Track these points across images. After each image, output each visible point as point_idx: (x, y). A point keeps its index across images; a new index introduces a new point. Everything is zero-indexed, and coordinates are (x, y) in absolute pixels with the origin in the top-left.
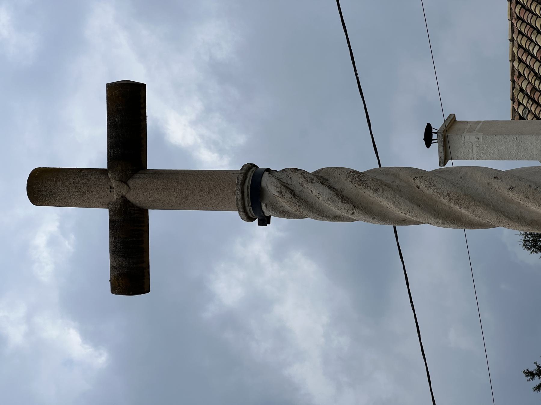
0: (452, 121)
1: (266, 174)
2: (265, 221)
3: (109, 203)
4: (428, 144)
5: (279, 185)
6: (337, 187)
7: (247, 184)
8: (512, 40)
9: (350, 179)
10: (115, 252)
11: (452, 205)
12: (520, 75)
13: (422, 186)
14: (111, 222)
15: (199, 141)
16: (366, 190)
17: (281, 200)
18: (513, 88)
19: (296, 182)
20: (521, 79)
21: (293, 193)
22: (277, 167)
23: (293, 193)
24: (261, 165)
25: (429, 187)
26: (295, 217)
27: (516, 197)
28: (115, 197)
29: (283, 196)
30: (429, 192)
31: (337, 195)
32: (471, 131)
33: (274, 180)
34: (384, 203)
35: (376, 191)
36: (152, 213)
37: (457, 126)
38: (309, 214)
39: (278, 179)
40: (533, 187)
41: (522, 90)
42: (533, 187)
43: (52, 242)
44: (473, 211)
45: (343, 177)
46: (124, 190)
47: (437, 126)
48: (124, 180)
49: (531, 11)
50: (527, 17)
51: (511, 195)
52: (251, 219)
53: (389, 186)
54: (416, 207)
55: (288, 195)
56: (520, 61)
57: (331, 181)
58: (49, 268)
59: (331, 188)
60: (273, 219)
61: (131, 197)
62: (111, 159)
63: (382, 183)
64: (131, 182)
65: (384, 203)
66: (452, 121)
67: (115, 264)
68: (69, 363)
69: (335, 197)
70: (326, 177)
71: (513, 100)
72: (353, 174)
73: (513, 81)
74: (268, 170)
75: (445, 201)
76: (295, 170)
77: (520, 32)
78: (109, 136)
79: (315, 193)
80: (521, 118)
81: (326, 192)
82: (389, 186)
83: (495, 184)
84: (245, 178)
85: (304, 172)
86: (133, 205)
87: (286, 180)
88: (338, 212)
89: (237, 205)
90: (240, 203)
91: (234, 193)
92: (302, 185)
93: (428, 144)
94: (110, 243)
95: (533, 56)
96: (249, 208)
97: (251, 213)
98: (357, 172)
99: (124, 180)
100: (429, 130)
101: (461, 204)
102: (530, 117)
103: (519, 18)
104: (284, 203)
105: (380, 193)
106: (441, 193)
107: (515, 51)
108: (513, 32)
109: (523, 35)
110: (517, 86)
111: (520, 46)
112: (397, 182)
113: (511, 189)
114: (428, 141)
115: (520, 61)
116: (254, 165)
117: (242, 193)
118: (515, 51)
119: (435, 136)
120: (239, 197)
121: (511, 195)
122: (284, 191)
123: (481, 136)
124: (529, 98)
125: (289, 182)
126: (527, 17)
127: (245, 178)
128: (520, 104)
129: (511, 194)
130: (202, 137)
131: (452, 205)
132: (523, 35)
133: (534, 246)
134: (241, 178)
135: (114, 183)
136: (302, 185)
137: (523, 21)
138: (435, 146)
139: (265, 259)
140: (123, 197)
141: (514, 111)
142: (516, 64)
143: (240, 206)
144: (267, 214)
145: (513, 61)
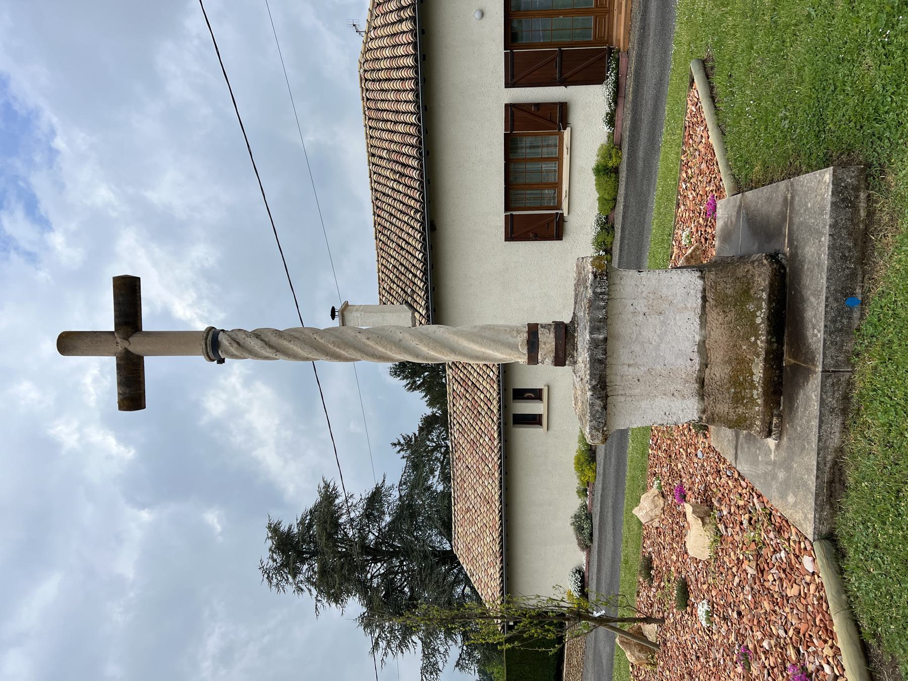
0: (346, 305)
1: (221, 333)
2: (221, 361)
3: (116, 353)
4: (333, 319)
5: (230, 339)
6: (266, 339)
7: (209, 339)
8: (378, 261)
9: (274, 335)
10: (120, 384)
11: (335, 348)
12: (383, 280)
13: (318, 338)
14: (118, 365)
15: (195, 316)
16: (284, 341)
17: (231, 348)
18: (380, 287)
19: (241, 337)
20: (384, 282)
21: (238, 343)
22: (228, 328)
23: (238, 343)
24: (218, 328)
25: (322, 338)
26: (241, 358)
27: (370, 343)
28: (120, 349)
29: (232, 346)
30: (322, 341)
31: (266, 344)
32: (357, 310)
33: (226, 336)
34: (295, 348)
35: (290, 341)
36: (145, 358)
37: (349, 308)
38: (249, 356)
39: (229, 336)
40: (380, 337)
41: (384, 288)
42: (380, 337)
43: (96, 380)
44: (347, 352)
45: (269, 334)
46: (126, 344)
47: (337, 308)
48: (126, 338)
49: (387, 245)
50: (386, 248)
51: (368, 342)
52: (213, 360)
53: (298, 338)
54: (314, 350)
55: (235, 345)
56: (383, 272)
57: (263, 336)
58: (93, 398)
59: (262, 340)
60: (226, 360)
61: (132, 349)
62: (116, 325)
63: (293, 336)
64: (131, 339)
65: (295, 348)
66: (346, 305)
67: (121, 392)
68: (109, 457)
69: (264, 346)
70: (259, 334)
71: (380, 294)
72: (277, 333)
73: (380, 284)
74: (223, 331)
75: (331, 346)
76: (240, 330)
77: (382, 257)
78: (115, 310)
79: (253, 343)
80: (384, 304)
81: (259, 343)
82: (298, 338)
83: (359, 336)
84: (207, 335)
85: (245, 331)
86: (132, 354)
87: (234, 336)
88: (267, 354)
89: (203, 352)
90: (204, 351)
91: (201, 345)
92: (244, 339)
93: (333, 319)
94: (118, 378)
95: (389, 270)
96: (211, 354)
97: (212, 357)
98: (278, 331)
99: (126, 338)
100: (333, 309)
101: (340, 348)
102: (389, 303)
103: (381, 249)
104: (233, 350)
105: (292, 342)
106: (329, 342)
107: (380, 267)
108: (378, 256)
109: (384, 258)
110: (381, 286)
111: (382, 264)
112: (303, 336)
113: (368, 339)
114: (333, 316)
115: (383, 272)
116: (214, 328)
117: (206, 344)
118: (380, 267)
119: (337, 314)
120: (204, 347)
121: (368, 342)
122: (232, 343)
123: (362, 313)
124: (388, 293)
125: (236, 337)
126: (386, 248)
127: (207, 335)
128: (383, 296)
129: (368, 341)
130: (196, 314)
131: (335, 348)
132: (384, 258)
133: (395, 374)
134: (205, 335)
135: (119, 340)
136: (244, 339)
137: (384, 251)
138: (337, 319)
139: (238, 386)
140: (125, 349)
141: (381, 300)
142: (380, 274)
143: (205, 352)
144: (222, 357)
145: (379, 272)
